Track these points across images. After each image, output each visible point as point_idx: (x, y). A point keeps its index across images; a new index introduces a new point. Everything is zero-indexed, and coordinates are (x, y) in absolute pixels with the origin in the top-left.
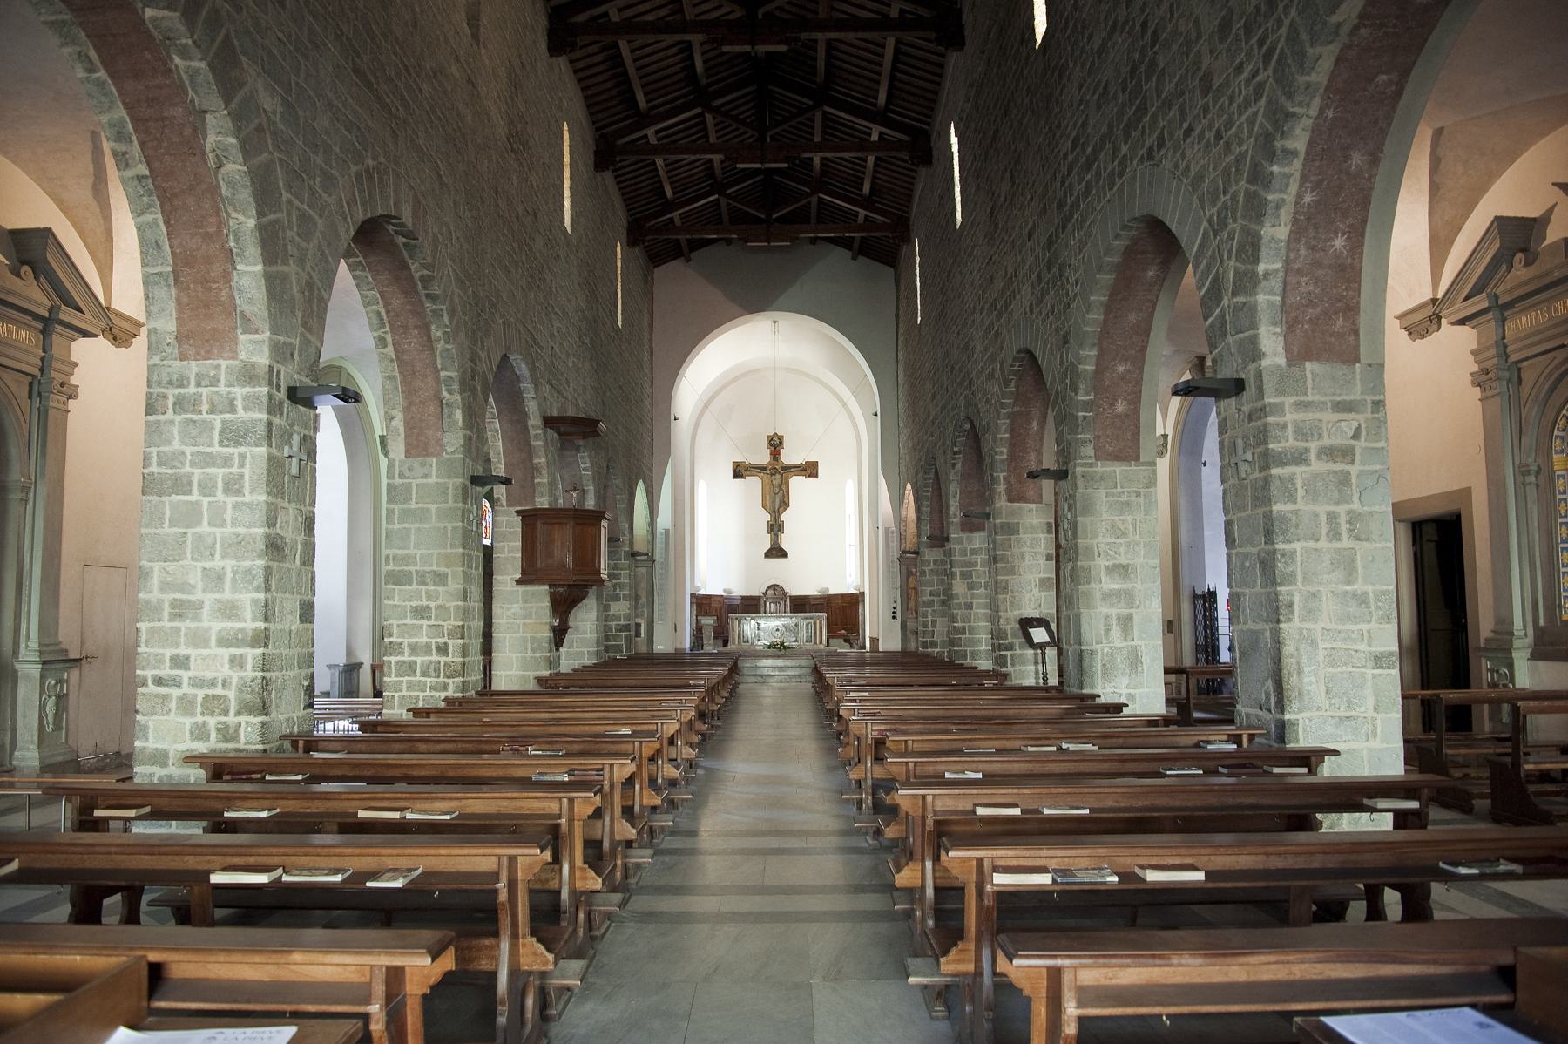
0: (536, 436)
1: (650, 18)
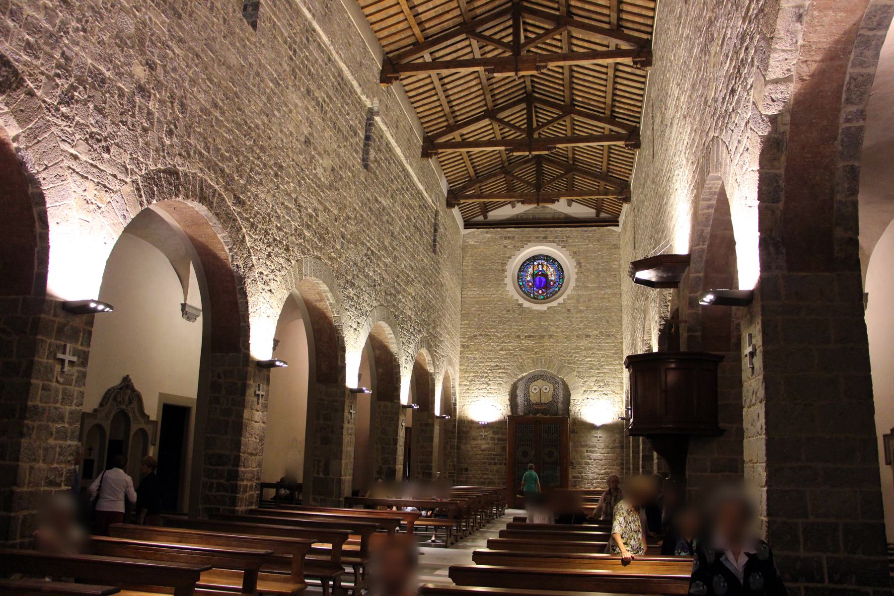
0: (16, 139)
1: (449, 58)
